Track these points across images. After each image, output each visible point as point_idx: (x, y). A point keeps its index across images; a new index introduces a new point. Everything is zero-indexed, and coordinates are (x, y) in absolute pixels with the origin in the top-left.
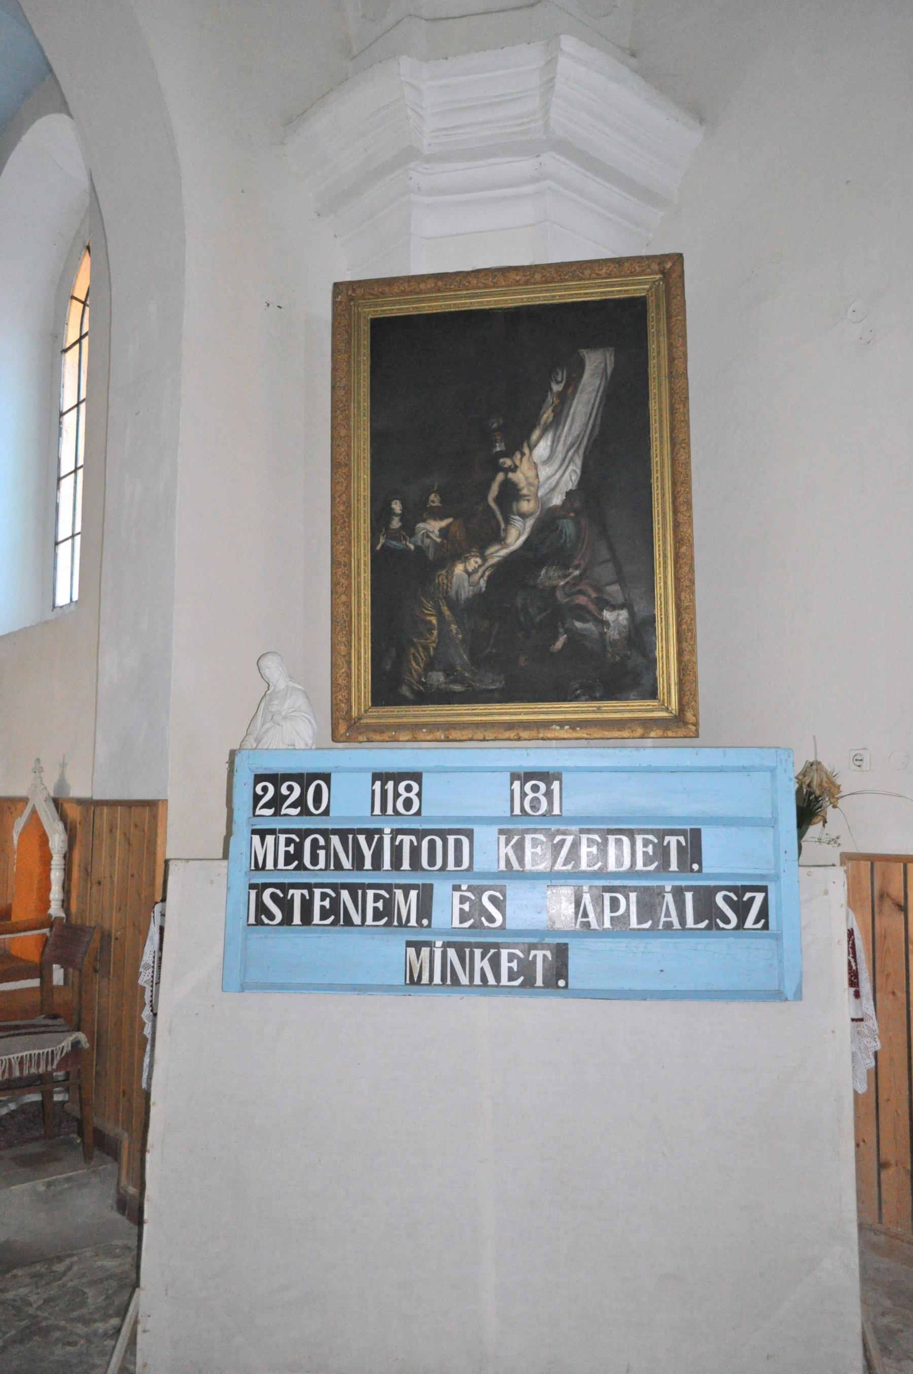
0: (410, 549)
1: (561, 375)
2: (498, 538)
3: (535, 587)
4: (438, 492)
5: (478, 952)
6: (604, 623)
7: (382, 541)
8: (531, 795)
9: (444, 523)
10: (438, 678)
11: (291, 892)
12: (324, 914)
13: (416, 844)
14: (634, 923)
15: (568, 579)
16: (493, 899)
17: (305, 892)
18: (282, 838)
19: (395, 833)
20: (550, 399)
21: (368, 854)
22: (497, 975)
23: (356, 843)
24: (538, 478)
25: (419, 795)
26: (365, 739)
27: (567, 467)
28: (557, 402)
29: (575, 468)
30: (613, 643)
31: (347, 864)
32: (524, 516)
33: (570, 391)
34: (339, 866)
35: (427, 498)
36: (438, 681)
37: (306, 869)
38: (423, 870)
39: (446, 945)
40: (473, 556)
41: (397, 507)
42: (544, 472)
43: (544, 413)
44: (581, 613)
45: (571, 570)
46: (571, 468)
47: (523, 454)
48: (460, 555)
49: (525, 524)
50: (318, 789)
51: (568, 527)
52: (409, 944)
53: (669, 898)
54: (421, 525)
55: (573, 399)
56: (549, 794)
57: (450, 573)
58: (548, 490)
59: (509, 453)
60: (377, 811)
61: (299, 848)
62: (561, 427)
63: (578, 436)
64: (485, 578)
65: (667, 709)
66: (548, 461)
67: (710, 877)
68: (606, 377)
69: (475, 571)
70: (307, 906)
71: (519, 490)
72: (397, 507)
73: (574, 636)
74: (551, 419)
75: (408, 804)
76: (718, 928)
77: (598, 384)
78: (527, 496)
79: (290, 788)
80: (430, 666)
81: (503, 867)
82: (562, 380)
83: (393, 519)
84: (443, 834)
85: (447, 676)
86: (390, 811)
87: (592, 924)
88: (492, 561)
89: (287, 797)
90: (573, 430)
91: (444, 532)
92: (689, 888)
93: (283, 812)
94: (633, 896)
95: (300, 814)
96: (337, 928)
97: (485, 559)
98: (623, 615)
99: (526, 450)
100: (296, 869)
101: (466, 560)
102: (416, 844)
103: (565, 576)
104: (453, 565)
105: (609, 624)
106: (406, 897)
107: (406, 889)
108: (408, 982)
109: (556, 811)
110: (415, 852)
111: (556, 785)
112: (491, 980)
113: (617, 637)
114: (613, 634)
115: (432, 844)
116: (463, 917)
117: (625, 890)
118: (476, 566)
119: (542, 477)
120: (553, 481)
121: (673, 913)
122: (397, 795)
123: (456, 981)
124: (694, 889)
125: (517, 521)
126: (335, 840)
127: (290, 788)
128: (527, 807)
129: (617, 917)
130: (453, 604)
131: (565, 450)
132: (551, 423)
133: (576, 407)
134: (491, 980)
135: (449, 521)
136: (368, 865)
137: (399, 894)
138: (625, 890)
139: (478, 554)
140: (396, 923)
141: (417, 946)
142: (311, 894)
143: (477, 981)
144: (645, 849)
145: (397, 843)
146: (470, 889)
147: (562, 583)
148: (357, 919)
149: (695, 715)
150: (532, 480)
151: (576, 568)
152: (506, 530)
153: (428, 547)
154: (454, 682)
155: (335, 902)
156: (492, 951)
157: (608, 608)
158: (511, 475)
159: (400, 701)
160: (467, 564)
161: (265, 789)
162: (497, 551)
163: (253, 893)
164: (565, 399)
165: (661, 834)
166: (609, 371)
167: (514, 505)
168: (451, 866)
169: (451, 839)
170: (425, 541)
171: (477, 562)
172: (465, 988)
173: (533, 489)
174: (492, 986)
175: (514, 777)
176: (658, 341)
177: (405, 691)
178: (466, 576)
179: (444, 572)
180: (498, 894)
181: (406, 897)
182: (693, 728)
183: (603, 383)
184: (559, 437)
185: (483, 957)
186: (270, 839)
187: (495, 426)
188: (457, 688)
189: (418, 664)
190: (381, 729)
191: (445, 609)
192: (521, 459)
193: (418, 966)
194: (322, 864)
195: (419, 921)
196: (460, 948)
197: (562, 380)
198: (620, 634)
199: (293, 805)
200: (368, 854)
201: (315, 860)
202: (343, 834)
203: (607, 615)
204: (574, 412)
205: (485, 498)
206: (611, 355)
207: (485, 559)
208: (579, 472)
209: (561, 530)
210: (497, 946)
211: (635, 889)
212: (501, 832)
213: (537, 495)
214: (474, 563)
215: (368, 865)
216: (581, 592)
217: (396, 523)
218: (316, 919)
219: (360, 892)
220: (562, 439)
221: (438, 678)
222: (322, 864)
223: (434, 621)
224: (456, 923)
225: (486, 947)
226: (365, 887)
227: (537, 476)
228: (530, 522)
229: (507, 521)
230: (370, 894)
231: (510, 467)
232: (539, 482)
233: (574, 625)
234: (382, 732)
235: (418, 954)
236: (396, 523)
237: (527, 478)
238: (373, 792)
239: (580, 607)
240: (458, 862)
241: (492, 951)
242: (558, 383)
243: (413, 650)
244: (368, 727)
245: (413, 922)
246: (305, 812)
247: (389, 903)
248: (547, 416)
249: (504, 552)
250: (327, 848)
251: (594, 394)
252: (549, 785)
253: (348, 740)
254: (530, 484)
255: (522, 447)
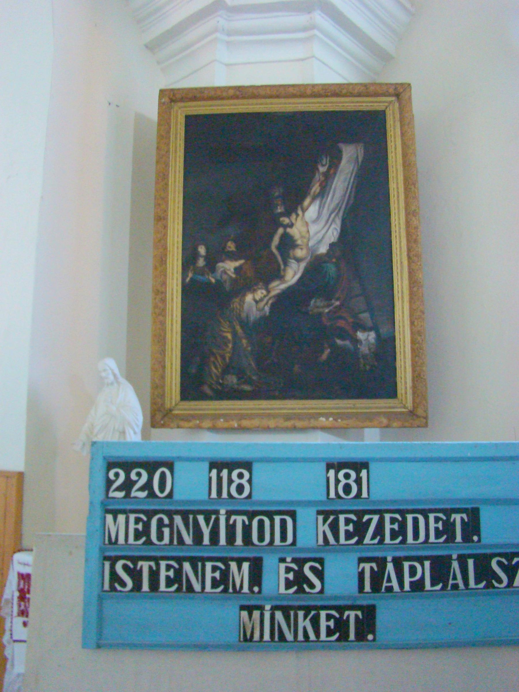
0: (211, 283)
1: (326, 161)
2: (279, 276)
3: (307, 313)
4: (235, 241)
5: (301, 614)
6: (356, 341)
7: (190, 275)
8: (343, 481)
9: (237, 264)
10: (232, 380)
11: (140, 563)
12: (169, 582)
13: (247, 523)
14: (428, 585)
15: (331, 308)
16: (313, 569)
17: (153, 564)
18: (132, 517)
19: (229, 514)
20: (317, 176)
21: (206, 532)
22: (317, 633)
23: (196, 523)
24: (309, 233)
25: (250, 481)
26: (176, 426)
27: (331, 224)
28: (322, 178)
29: (336, 226)
30: (364, 357)
31: (188, 539)
32: (299, 260)
33: (332, 171)
34: (181, 541)
35: (226, 245)
36: (232, 382)
37: (152, 543)
38: (253, 544)
39: (274, 608)
40: (259, 289)
41: (202, 250)
42: (313, 229)
43: (313, 186)
44: (343, 334)
45: (333, 301)
46: (333, 226)
47: (297, 215)
48: (250, 288)
49: (299, 266)
50: (163, 476)
51: (331, 269)
52: (243, 608)
53: (455, 565)
54: (220, 264)
55: (334, 178)
56: (358, 481)
57: (242, 302)
58: (316, 242)
59: (288, 213)
60: (214, 495)
61: (147, 526)
62: (325, 197)
63: (338, 204)
64: (269, 305)
65: (404, 407)
66: (315, 221)
67: (486, 546)
68: (358, 164)
69: (261, 300)
70: (154, 575)
71: (296, 241)
72: (202, 250)
73: (335, 349)
74: (318, 190)
75: (240, 489)
76: (494, 587)
77: (352, 168)
78: (301, 245)
79: (139, 475)
80: (227, 370)
81: (321, 541)
82: (326, 163)
83: (199, 259)
84: (270, 515)
85: (239, 378)
86: (225, 495)
87: (394, 588)
88: (273, 293)
89: (136, 482)
90: (334, 199)
91: (237, 270)
92: (470, 556)
93: (133, 494)
94: (427, 564)
95: (148, 497)
96: (181, 595)
97: (268, 292)
98: (372, 336)
99: (300, 212)
100: (144, 543)
101: (254, 291)
102: (247, 523)
103: (328, 306)
104: (244, 295)
105: (362, 342)
106: (240, 568)
107: (240, 561)
108: (242, 639)
109: (365, 494)
110: (247, 530)
111: (364, 473)
112: (312, 636)
113: (367, 351)
114: (364, 349)
115: (261, 523)
116: (289, 584)
117: (421, 560)
118: (262, 296)
119: (312, 232)
120: (320, 236)
121: (459, 576)
122: (230, 481)
123: (282, 638)
124: (476, 557)
125: (293, 264)
126: (178, 520)
127: (139, 475)
128: (341, 492)
129: (414, 581)
130: (244, 324)
131: (329, 212)
132: (319, 193)
133: (337, 183)
134: (312, 636)
135: (242, 262)
136: (206, 540)
137: (233, 565)
138: (421, 560)
139: (264, 287)
140: (231, 590)
141: (250, 609)
142: (158, 565)
143: (301, 637)
144: (436, 525)
145: (231, 522)
146: (294, 560)
147: (327, 311)
148: (197, 587)
149: (425, 411)
150: (304, 234)
151: (338, 299)
152: (284, 270)
153: (225, 281)
154: (246, 383)
155: (179, 572)
156: (313, 613)
157: (360, 329)
158: (289, 230)
159: (204, 397)
160: (255, 294)
161: (117, 475)
162: (278, 285)
163: (107, 564)
164: (328, 177)
165: (448, 512)
166: (360, 160)
167: (291, 253)
168: (277, 541)
169: (277, 519)
170: (223, 277)
171: (262, 293)
172: (198, 594)
173: (305, 240)
174: (312, 641)
175: (329, 466)
176: (395, 141)
177: (206, 389)
178: (254, 303)
179: (237, 300)
180: (317, 565)
181: (240, 568)
182: (424, 421)
183: (355, 169)
184: (324, 205)
185: (305, 617)
186: (121, 518)
187: (277, 194)
188: (247, 388)
189: (216, 368)
190: (187, 418)
191: (238, 329)
192: (296, 219)
193: (251, 626)
194: (166, 540)
195: (251, 588)
196: (286, 610)
197: (326, 163)
198: (370, 349)
199: (142, 489)
200: (206, 532)
201: (160, 537)
202: (185, 515)
203: (360, 335)
204: (335, 188)
205: (268, 245)
206: (361, 149)
207: (268, 292)
208: (339, 229)
209: (326, 272)
210: (315, 608)
211: (427, 558)
212: (319, 513)
213: (308, 245)
214: (260, 294)
215: (206, 540)
216: (341, 318)
217: (201, 262)
218: (162, 587)
219: (200, 564)
220: (326, 206)
221: (232, 380)
222: (166, 540)
223: (229, 336)
224: (282, 589)
225: (307, 609)
226: (204, 560)
227: (308, 232)
228: (303, 265)
229: (286, 263)
230: (209, 565)
231: (288, 224)
232: (309, 235)
233: (335, 342)
234: (189, 421)
235: (250, 615)
236: (201, 262)
237: (300, 233)
238: (210, 479)
239: (341, 328)
240: (284, 538)
241: (313, 613)
242: (323, 166)
243: (212, 359)
244: (177, 416)
245: (246, 589)
246: (152, 495)
247: (225, 574)
248: (316, 188)
249: (283, 286)
250: (171, 526)
251: (349, 175)
252: (358, 473)
253: (163, 426)
254: (302, 237)
255: (297, 209)
